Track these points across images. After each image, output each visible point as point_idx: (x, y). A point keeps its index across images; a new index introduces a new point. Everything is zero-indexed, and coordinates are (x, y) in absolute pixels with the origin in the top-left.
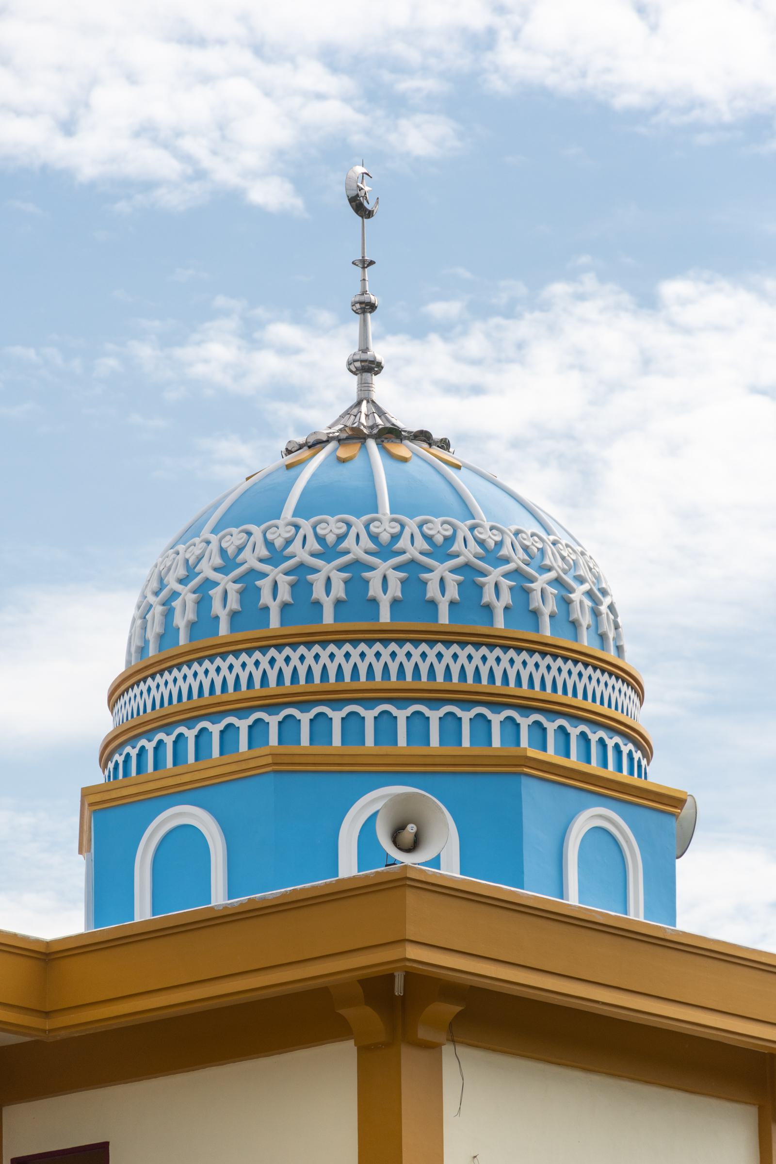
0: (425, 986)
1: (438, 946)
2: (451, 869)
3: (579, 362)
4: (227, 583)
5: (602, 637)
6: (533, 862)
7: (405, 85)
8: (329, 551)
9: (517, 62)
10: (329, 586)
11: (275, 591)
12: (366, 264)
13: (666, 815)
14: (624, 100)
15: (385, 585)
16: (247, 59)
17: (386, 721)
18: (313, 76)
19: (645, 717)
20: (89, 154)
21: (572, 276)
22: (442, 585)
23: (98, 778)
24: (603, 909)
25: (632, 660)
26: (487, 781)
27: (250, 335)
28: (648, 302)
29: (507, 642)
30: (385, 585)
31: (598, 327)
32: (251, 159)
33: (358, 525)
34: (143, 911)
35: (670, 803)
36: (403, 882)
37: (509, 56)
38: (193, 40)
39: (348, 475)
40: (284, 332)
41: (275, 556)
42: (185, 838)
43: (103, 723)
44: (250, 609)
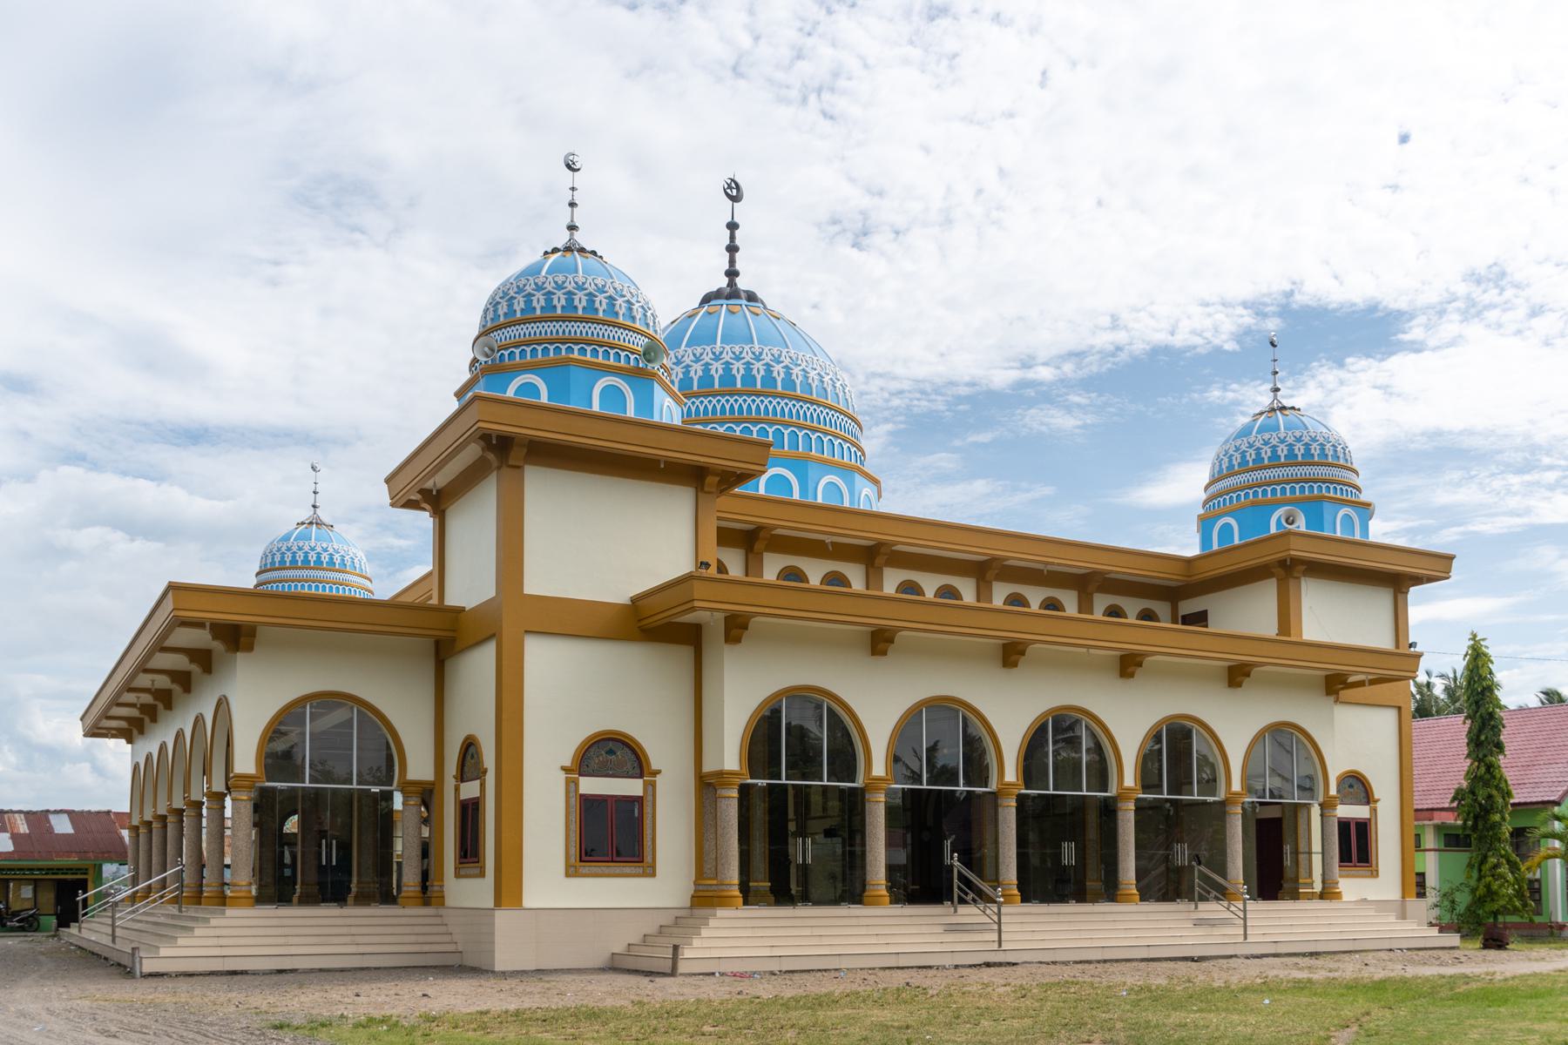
0: (1296, 561)
1: (1299, 551)
2: (1303, 529)
3: (1321, 385)
6: (1326, 525)
7: (1267, 309)
8: (1266, 443)
9: (1299, 299)
11: (1251, 455)
12: (573, 189)
13: (1366, 509)
14: (1330, 307)
15: (1283, 451)
16: (1221, 308)
17: (1265, 492)
18: (1240, 310)
19: (1358, 482)
20: (1179, 340)
21: (1319, 360)
22: (1299, 450)
23: (1202, 511)
25: (1355, 466)
26: (1314, 505)
27: (1225, 389)
28: (1341, 364)
29: (1318, 464)
30: (1283, 451)
31: (1329, 376)
32: (1224, 337)
34: (1215, 547)
35: (1367, 505)
36: (1289, 533)
37: (1298, 297)
38: (1207, 305)
39: (1272, 421)
40: (1235, 386)
41: (1251, 446)
42: (1228, 526)
43: (1204, 496)
44: (1244, 462)
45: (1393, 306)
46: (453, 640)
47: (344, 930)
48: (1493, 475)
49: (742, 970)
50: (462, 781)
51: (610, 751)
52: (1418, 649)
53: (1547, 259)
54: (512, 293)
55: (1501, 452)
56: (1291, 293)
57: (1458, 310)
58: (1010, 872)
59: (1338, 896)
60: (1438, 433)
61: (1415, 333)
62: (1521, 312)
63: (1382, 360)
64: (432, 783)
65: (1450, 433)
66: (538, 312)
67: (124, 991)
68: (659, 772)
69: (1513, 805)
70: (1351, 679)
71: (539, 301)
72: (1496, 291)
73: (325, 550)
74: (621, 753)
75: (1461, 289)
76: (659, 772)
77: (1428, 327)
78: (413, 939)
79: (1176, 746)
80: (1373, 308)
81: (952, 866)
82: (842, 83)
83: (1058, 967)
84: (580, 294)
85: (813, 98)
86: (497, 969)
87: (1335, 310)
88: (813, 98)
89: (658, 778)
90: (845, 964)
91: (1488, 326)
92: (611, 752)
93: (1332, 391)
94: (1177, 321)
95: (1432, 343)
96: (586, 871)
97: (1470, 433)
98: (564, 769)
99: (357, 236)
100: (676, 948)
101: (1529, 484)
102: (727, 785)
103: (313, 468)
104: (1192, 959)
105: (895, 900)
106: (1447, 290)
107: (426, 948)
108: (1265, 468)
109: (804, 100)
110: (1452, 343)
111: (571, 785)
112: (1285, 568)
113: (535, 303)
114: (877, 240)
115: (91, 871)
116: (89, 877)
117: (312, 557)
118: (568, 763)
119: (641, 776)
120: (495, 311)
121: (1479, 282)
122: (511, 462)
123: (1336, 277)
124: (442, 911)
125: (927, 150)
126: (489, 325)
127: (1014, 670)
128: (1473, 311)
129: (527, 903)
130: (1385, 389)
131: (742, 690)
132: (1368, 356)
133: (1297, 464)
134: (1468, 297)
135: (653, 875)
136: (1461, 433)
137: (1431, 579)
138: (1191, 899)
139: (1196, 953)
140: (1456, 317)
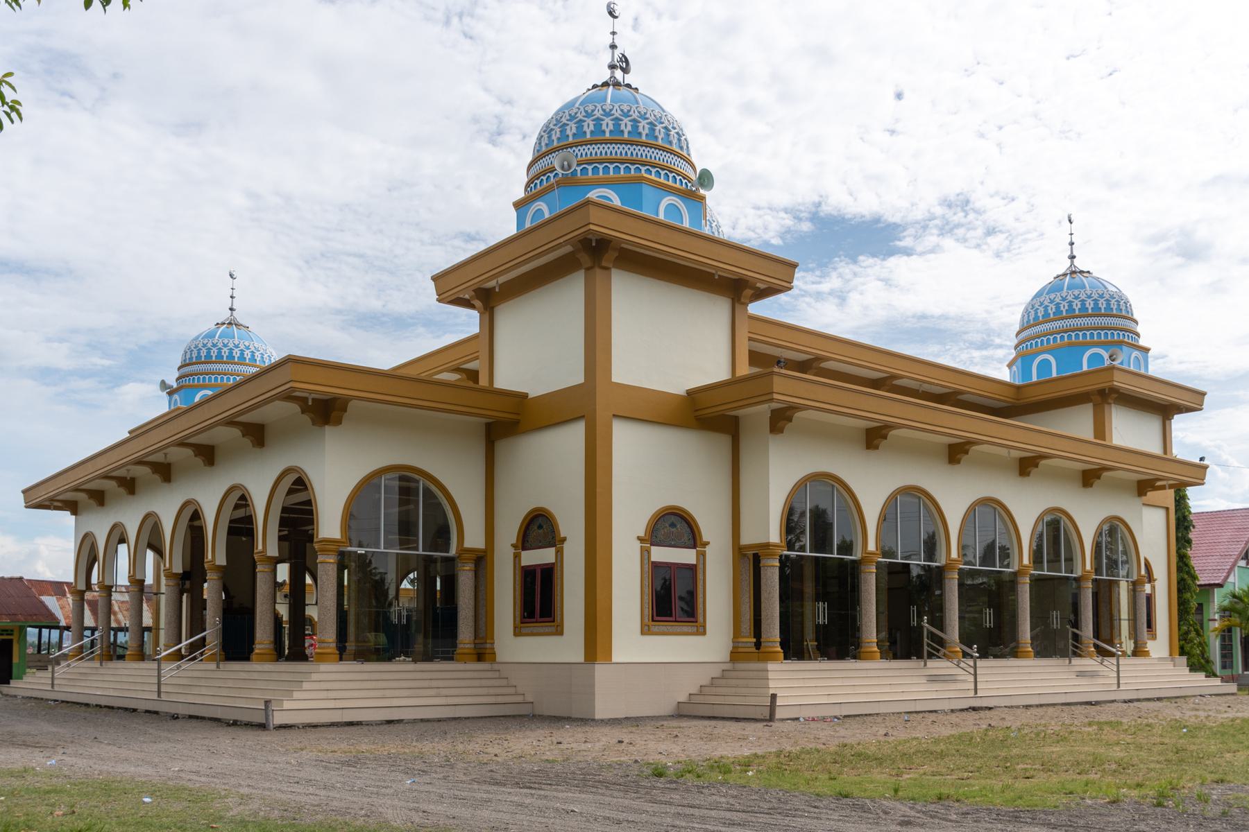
0: (1114, 390)
1: (1120, 382)
3: (840, 276)
4: (1042, 309)
5: (681, 148)
8: (1076, 298)
9: (826, 209)
10: (1077, 306)
12: (614, 33)
15: (1090, 305)
18: (782, 215)
19: (1139, 329)
22: (1102, 304)
24: (1136, 370)
28: (855, 262)
30: (1090, 305)
31: (846, 269)
33: (634, 107)
35: (1147, 350)
36: (1112, 368)
38: (758, 208)
44: (1046, 314)
45: (892, 220)
46: (517, 423)
47: (426, 684)
48: (961, 349)
49: (812, 715)
50: (524, 549)
51: (673, 525)
52: (1206, 462)
53: (997, 193)
54: (564, 120)
55: (966, 333)
56: (820, 204)
57: (936, 226)
58: (953, 632)
59: (1146, 654)
60: (923, 317)
61: (907, 242)
62: (980, 232)
63: (884, 259)
64: (485, 551)
65: (932, 317)
66: (588, 136)
67: (264, 737)
68: (708, 543)
69: (1200, 586)
70: (1159, 483)
71: (589, 127)
72: (962, 214)
73: (248, 348)
74: (681, 526)
75: (939, 211)
76: (708, 543)
77: (916, 237)
78: (485, 691)
79: (1055, 530)
80: (877, 220)
81: (921, 628)
82: (479, 11)
83: (1044, 709)
84: (644, 123)
85: (455, 20)
86: (597, 717)
87: (850, 219)
88: (455, 20)
89: (708, 549)
90: (883, 709)
91: (957, 240)
92: (673, 525)
93: (849, 280)
94: (737, 219)
95: (919, 249)
96: (655, 629)
97: (945, 317)
98: (639, 538)
99: (67, 100)
100: (267, 702)
101: (986, 358)
102: (771, 555)
103: (231, 276)
104: (1089, 703)
105: (884, 656)
106: (929, 211)
107: (500, 699)
108: (1077, 317)
109: (447, 22)
110: (932, 251)
111: (645, 553)
112: (1104, 394)
113: (585, 128)
114: (507, 139)
115: (16, 633)
116: (15, 638)
117: (237, 353)
118: (642, 534)
119: (694, 547)
120: (549, 137)
121: (950, 206)
122: (604, 264)
123: (851, 195)
124: (496, 666)
125: (547, 72)
126: (544, 149)
127: (957, 466)
128: (947, 229)
129: (614, 660)
130: (887, 282)
131: (780, 473)
132: (874, 255)
133: (1101, 315)
134: (943, 217)
135: (704, 633)
136: (940, 317)
137: (1189, 410)
138: (920, 657)
139: (1093, 698)
140: (935, 231)
